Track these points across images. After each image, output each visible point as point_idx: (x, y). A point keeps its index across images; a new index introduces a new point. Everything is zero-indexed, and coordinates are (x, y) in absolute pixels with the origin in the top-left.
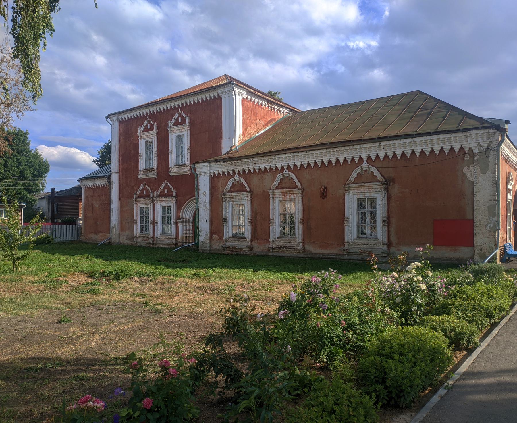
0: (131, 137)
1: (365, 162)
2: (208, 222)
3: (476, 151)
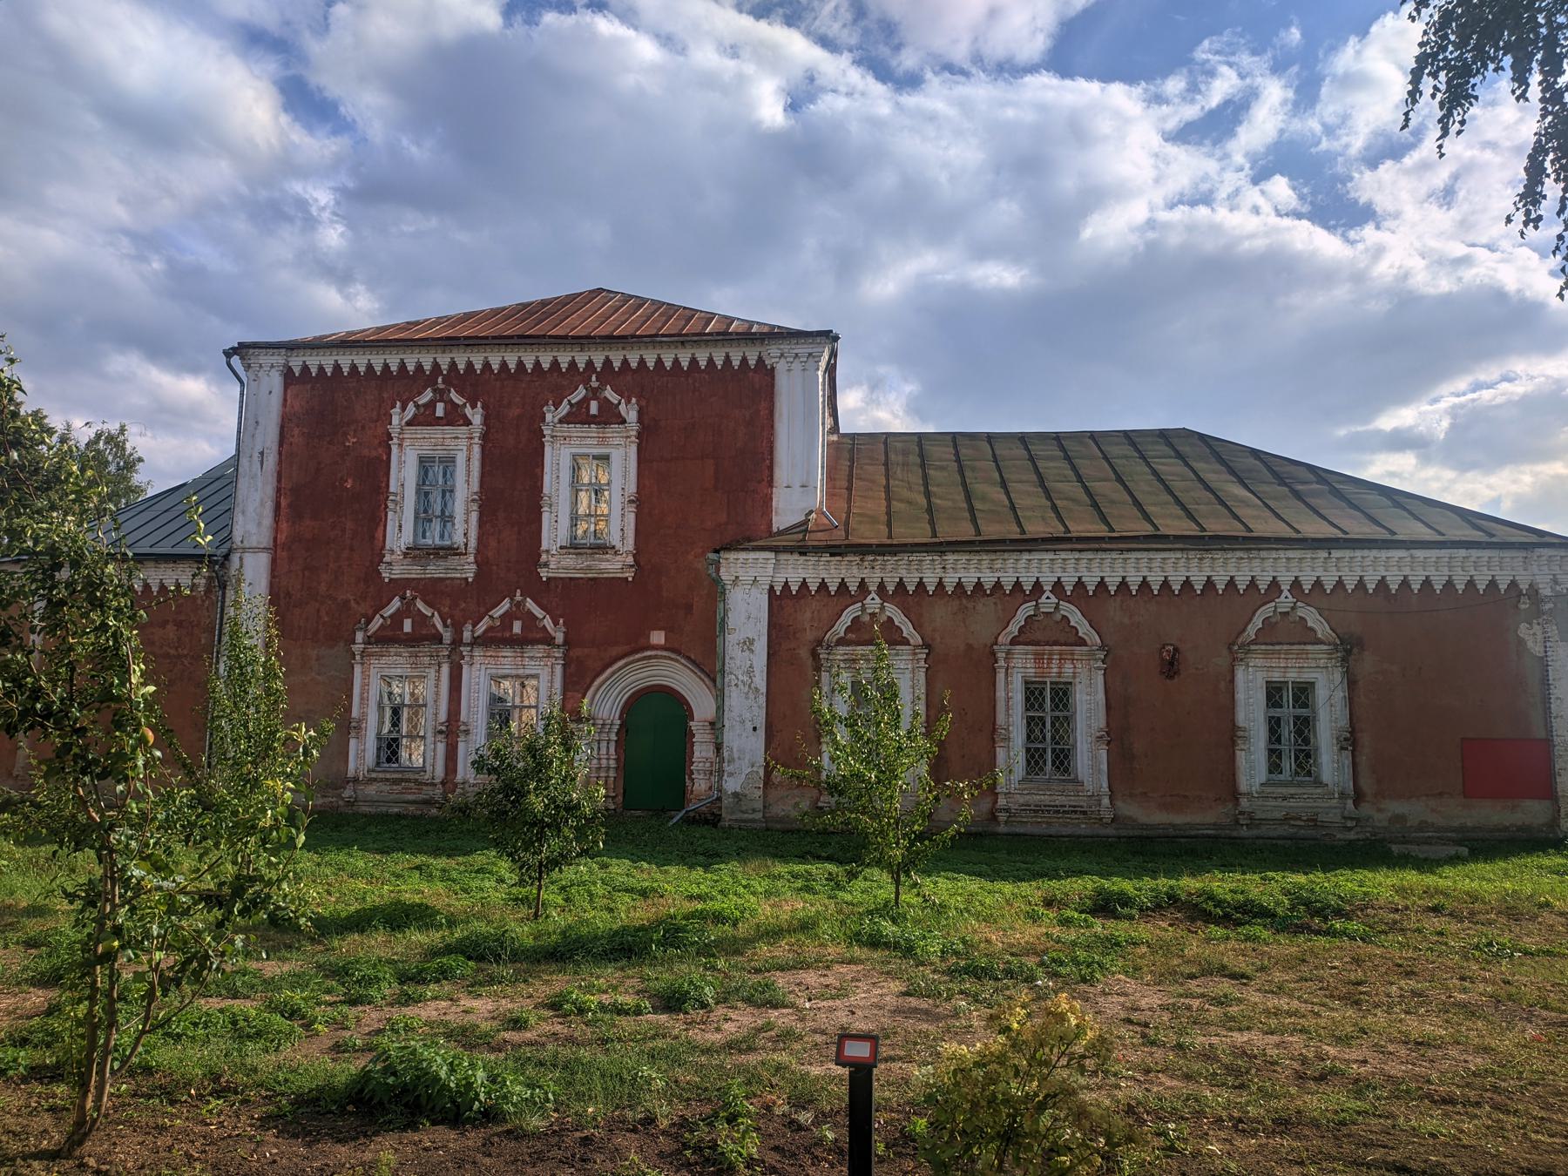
0: (345, 434)
1: (1286, 593)
2: (762, 733)
3: (1546, 591)
